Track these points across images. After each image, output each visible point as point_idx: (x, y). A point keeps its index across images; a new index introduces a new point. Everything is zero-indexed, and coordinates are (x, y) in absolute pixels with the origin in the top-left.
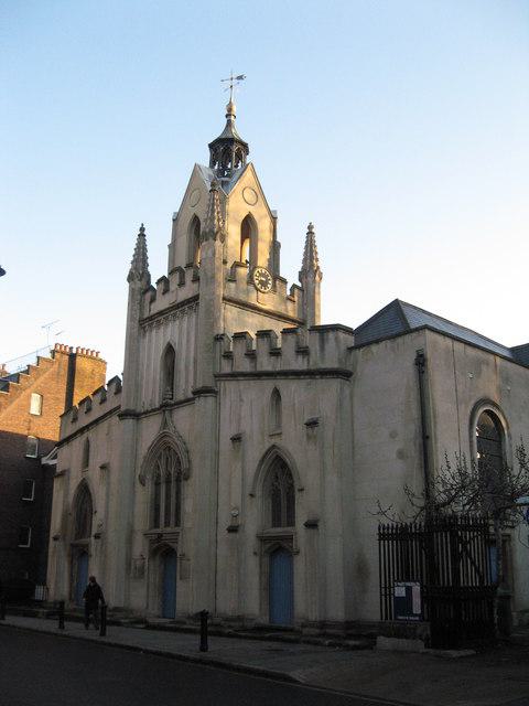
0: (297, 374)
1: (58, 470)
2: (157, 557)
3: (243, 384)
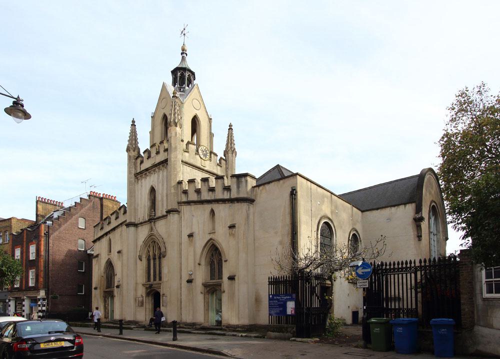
0: (224, 201)
3: (193, 207)
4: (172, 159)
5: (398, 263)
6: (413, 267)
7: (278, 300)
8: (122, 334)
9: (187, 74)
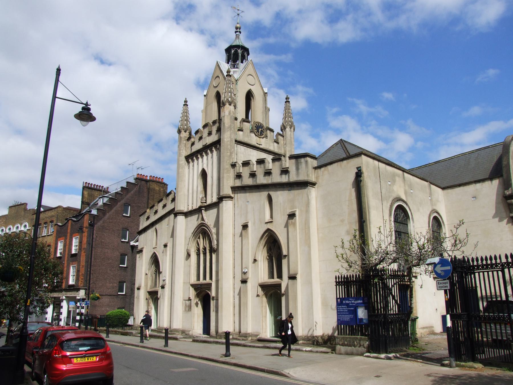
1: (139, 248)
4: (225, 140)
5: (482, 259)
6: (499, 264)
7: (347, 305)
8: (167, 346)
9: (240, 51)
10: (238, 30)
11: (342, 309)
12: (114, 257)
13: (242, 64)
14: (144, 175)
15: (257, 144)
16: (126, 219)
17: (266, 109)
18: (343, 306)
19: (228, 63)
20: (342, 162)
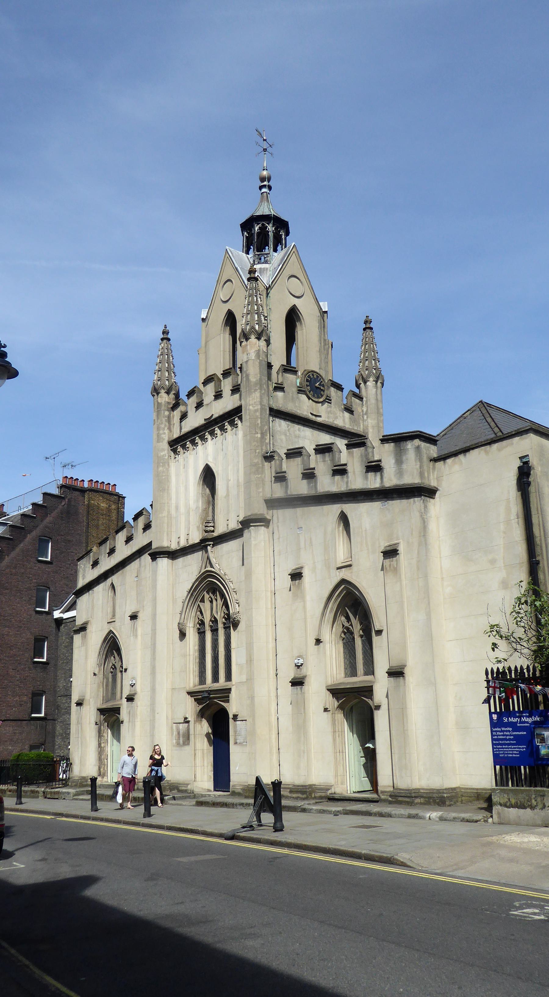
2: (405, 448)
7: (513, 725)
9: (270, 228)
10: (266, 183)
11: (502, 733)
12: (22, 643)
13: (275, 254)
14: (77, 479)
15: (312, 414)
16: (43, 566)
17: (325, 345)
18: (503, 729)
19: (247, 253)
20: (488, 446)
